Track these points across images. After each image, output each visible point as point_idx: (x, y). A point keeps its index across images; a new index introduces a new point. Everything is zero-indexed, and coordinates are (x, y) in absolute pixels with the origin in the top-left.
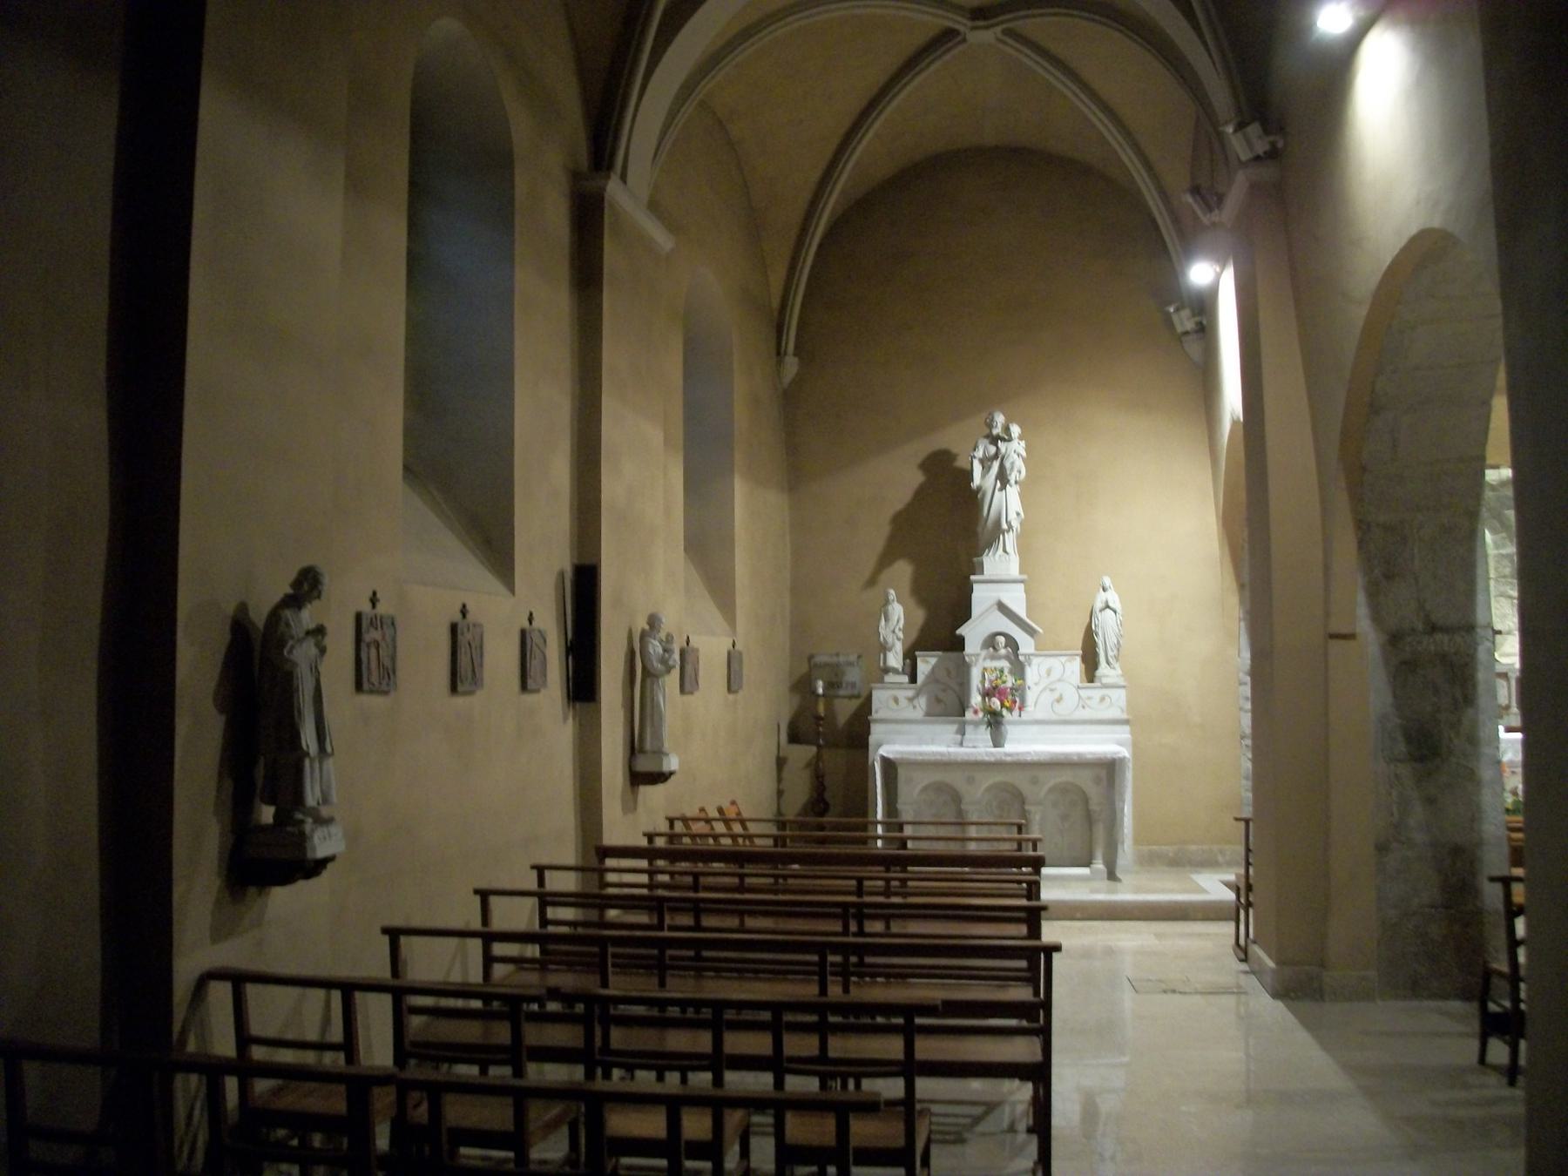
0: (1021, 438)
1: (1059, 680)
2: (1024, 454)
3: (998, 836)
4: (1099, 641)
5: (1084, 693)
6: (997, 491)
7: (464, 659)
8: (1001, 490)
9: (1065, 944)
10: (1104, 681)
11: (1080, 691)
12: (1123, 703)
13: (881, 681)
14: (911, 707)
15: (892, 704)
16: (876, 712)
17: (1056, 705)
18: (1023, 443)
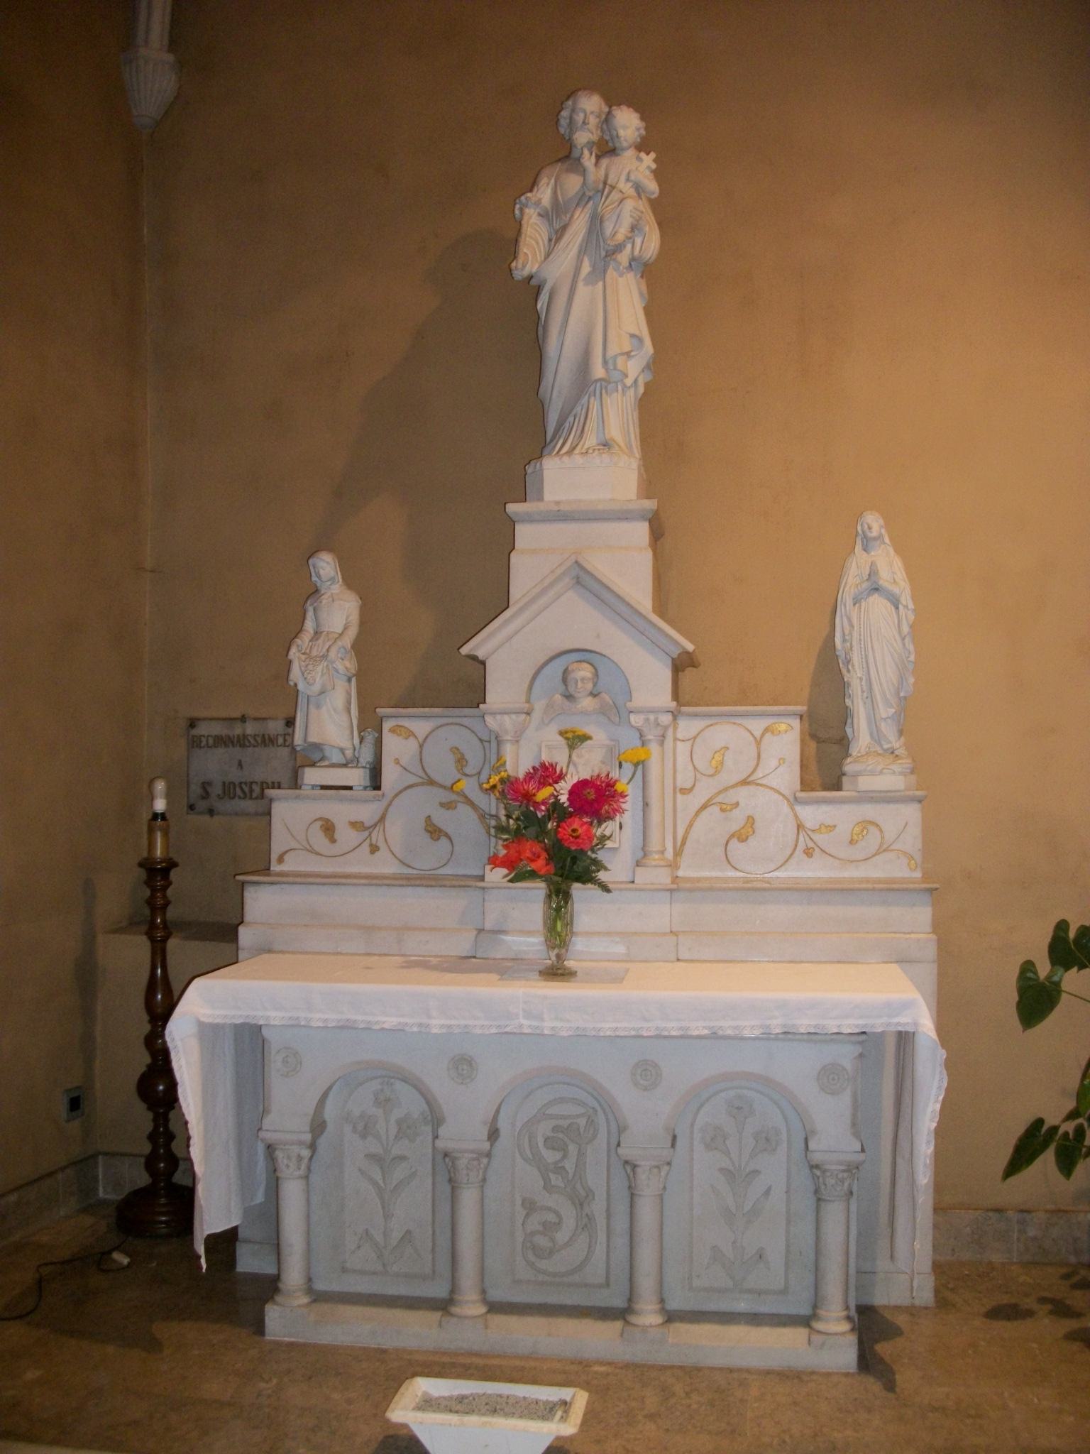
0: (643, 146)
1: (745, 782)
2: (652, 186)
3: (601, 292)
4: (855, 678)
5: (812, 815)
6: (580, 284)
7: (424, 715)
8: (590, 280)
9: (594, 738)
10: (865, 783)
11: (798, 808)
12: (912, 840)
13: (295, 784)
14: (366, 847)
15: (319, 840)
16: (281, 860)
17: (734, 844)
18: (648, 160)
